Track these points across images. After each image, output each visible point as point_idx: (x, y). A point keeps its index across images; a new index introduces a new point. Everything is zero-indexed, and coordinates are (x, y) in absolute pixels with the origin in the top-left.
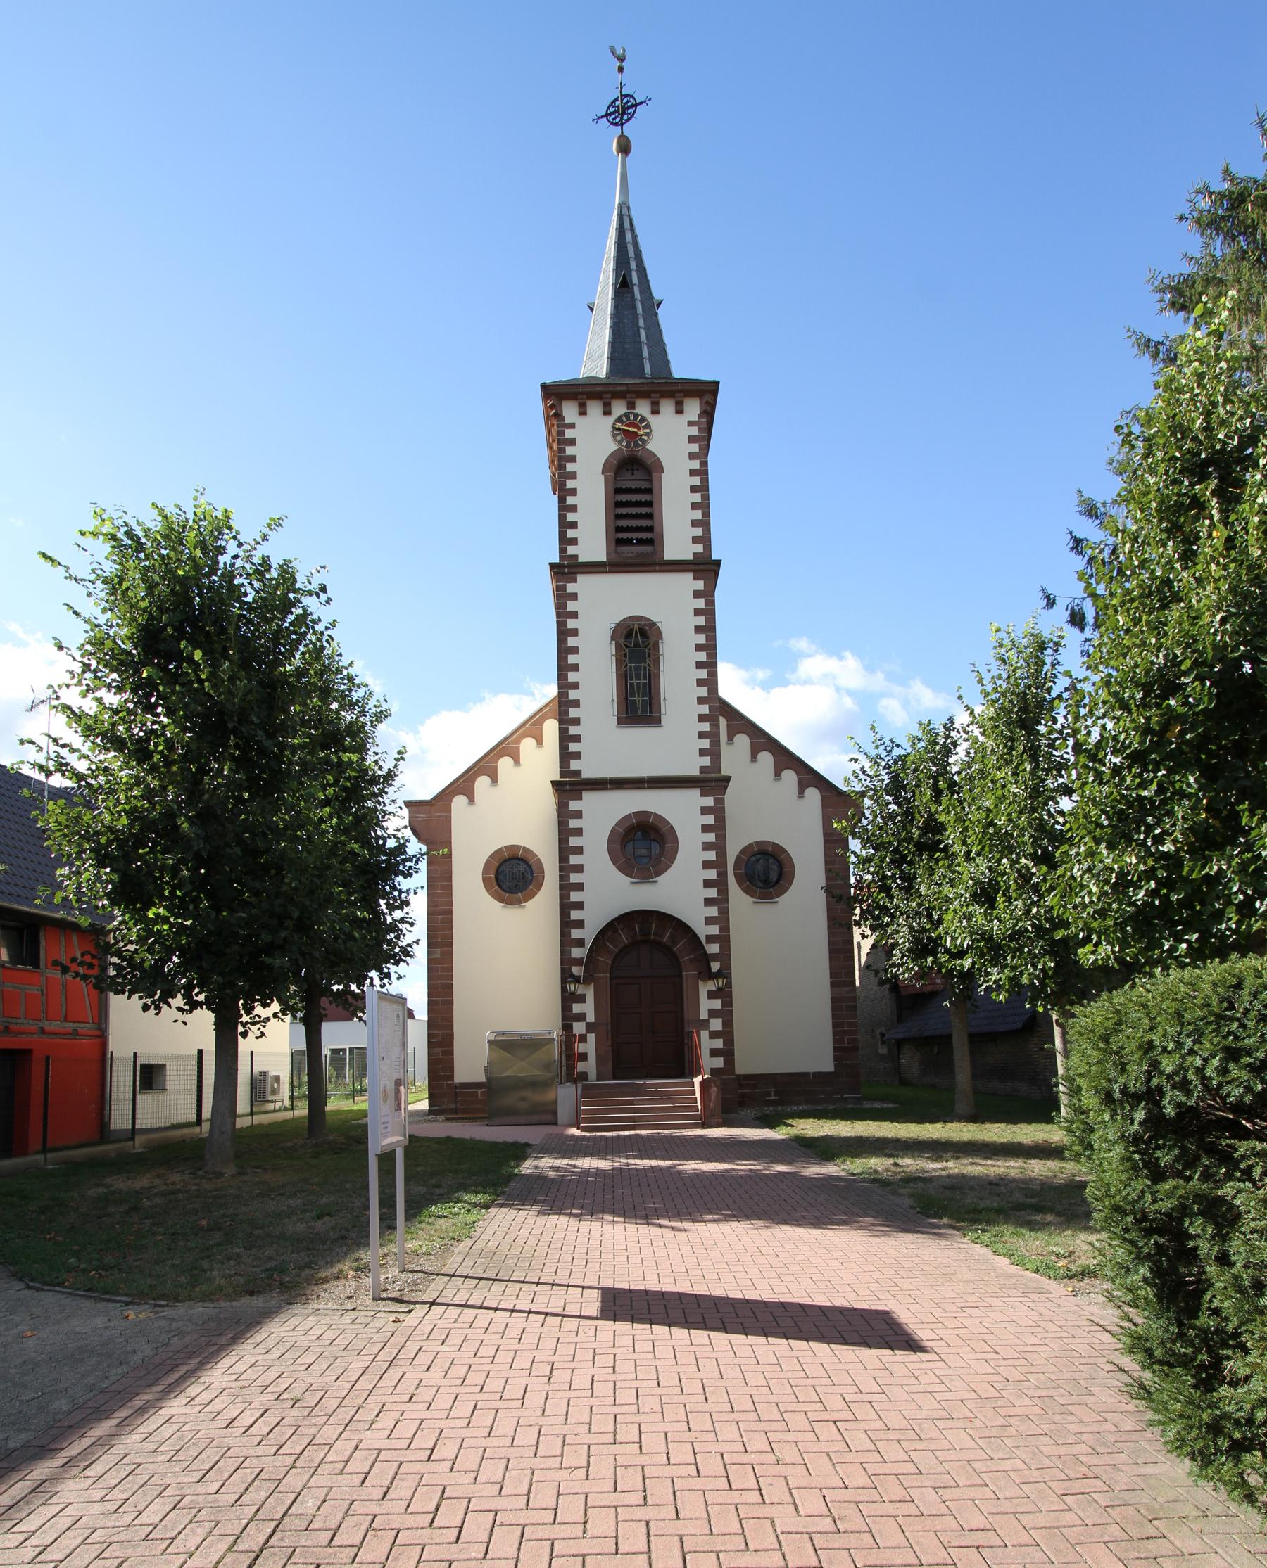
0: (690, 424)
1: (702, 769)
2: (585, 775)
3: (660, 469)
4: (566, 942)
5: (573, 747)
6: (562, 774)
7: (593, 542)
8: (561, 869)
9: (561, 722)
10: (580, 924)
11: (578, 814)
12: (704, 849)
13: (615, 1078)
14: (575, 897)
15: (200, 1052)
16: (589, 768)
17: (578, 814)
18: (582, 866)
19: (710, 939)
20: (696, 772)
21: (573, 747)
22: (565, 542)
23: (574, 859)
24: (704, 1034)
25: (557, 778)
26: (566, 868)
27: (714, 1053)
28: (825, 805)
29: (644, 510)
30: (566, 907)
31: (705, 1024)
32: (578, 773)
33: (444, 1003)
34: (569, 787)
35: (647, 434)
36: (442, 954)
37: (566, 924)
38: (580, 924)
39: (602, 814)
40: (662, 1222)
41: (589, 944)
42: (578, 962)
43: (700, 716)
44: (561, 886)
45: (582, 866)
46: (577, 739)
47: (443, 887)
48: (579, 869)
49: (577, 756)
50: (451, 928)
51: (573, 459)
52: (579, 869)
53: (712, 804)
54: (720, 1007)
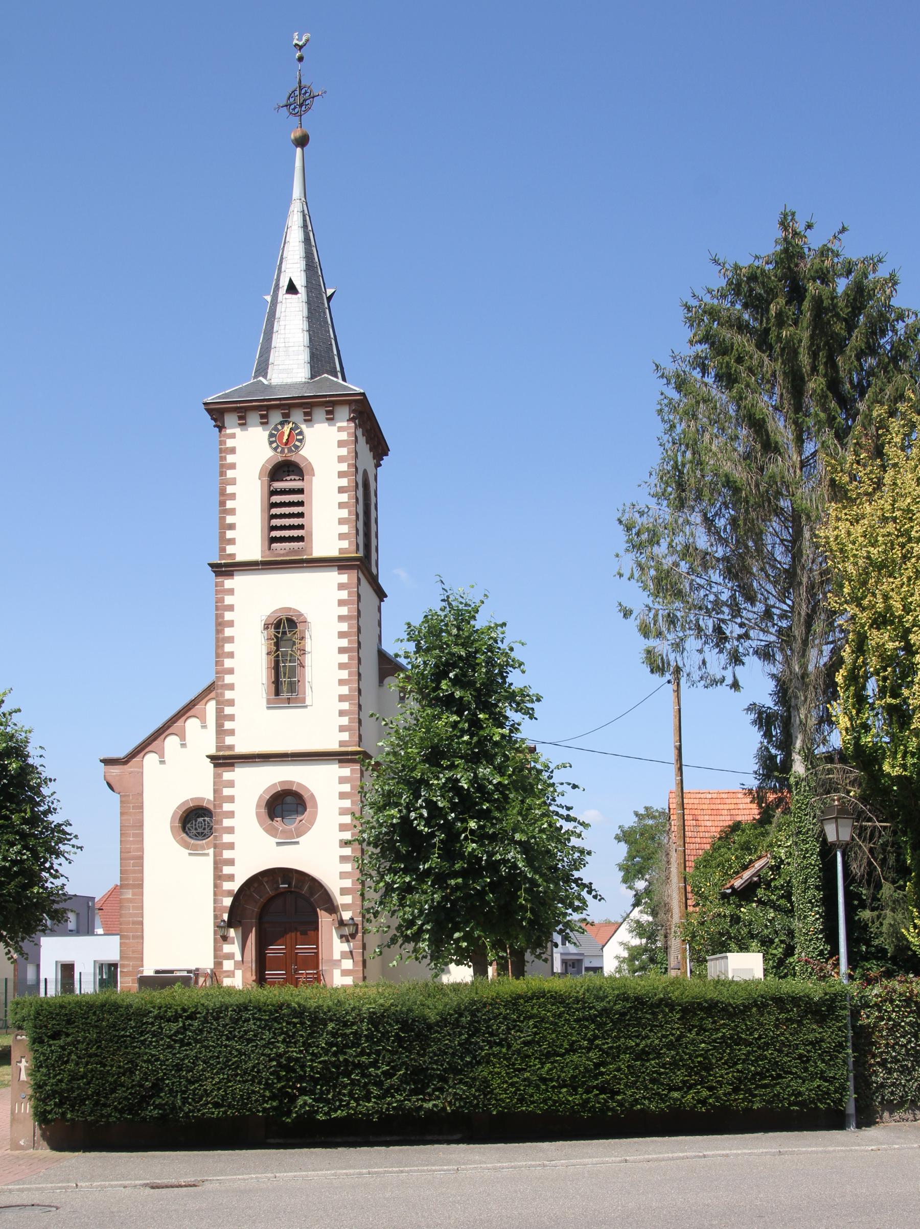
0: (340, 429)
6: (218, 748)
7: (248, 542)
9: (218, 703)
10: (231, 878)
11: (231, 784)
12: (340, 731)
15: (6, 979)
17: (231, 784)
19: (344, 891)
22: (221, 732)
24: (337, 973)
25: (213, 751)
29: (296, 510)
32: (231, 747)
33: (134, 937)
34: (224, 760)
35: (300, 441)
36: (133, 894)
39: (251, 785)
40: (288, 478)
47: (135, 835)
49: (232, 732)
50: (142, 872)
51: (231, 608)
54: (350, 902)
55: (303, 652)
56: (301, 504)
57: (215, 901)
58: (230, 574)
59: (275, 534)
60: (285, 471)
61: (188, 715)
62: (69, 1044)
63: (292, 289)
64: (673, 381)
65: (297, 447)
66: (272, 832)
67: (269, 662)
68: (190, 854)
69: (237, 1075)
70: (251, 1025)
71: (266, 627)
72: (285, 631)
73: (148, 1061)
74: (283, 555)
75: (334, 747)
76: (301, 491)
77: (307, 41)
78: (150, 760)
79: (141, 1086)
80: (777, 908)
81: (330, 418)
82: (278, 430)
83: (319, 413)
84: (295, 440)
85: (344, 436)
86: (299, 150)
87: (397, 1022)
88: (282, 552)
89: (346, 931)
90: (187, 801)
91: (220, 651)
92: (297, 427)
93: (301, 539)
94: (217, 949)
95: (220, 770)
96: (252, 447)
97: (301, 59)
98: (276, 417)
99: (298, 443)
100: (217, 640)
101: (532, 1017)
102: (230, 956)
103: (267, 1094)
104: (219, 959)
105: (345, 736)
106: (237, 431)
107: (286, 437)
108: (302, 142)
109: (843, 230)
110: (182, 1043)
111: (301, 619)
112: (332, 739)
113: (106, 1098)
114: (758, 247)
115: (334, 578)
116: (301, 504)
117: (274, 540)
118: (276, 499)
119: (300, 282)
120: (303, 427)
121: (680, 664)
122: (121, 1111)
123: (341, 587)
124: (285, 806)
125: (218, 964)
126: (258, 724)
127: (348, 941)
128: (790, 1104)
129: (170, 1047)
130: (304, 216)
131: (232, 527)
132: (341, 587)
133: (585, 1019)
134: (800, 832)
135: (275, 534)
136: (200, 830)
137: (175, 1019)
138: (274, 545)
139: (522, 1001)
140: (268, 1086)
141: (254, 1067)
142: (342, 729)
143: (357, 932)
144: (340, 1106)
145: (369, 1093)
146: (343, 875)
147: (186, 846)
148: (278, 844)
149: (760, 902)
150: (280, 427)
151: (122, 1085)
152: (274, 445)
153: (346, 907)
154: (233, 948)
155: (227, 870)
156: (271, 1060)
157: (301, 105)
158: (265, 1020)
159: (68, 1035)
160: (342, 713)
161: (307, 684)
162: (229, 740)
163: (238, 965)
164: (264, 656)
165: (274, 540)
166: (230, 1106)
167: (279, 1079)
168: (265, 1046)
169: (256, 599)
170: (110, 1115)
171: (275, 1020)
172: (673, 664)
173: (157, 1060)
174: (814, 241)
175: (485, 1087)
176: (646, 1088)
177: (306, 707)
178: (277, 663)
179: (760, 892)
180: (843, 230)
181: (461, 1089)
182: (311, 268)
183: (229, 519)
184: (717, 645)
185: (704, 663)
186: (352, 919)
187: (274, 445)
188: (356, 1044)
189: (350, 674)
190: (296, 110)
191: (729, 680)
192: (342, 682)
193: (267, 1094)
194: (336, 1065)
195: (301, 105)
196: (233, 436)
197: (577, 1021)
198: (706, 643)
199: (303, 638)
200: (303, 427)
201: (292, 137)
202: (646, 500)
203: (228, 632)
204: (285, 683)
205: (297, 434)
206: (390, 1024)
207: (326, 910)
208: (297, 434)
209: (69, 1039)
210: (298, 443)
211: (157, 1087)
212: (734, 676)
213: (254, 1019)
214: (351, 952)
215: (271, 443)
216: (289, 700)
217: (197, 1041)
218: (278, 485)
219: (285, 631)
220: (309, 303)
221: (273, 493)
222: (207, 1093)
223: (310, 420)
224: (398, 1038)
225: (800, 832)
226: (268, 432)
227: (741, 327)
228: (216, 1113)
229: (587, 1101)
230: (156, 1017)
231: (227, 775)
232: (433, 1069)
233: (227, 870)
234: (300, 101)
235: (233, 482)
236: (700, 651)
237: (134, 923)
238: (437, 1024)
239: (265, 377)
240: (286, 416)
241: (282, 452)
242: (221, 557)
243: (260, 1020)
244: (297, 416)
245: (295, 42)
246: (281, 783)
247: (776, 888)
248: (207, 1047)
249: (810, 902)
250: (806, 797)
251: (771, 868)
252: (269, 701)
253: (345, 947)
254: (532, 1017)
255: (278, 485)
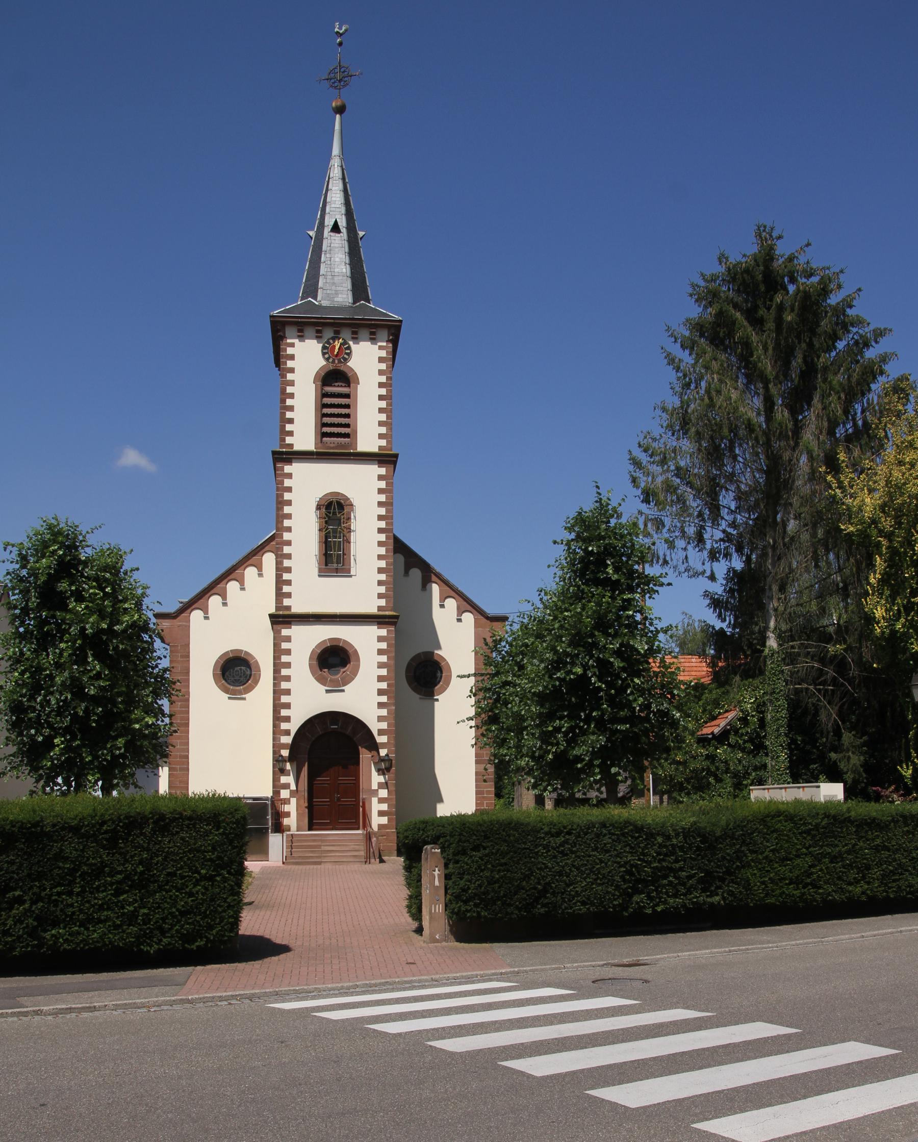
0: (381, 348)
1: (380, 448)
2: (296, 448)
3: (357, 382)
4: (277, 732)
5: (286, 589)
6: (277, 608)
7: (304, 435)
8: (275, 678)
10: (287, 719)
13: (310, 829)
14: (284, 699)
16: (297, 606)
18: (290, 581)
19: (381, 732)
20: (376, 450)
21: (286, 589)
22: (280, 595)
23: (284, 672)
24: (375, 800)
26: (278, 666)
27: (381, 813)
28: (477, 625)
30: (278, 706)
31: (375, 793)
32: (289, 608)
33: (181, 769)
34: (282, 619)
37: (278, 719)
38: (287, 719)
39: (306, 640)
41: (293, 734)
42: (284, 746)
43: (379, 569)
44: (274, 745)
45: (290, 581)
46: (289, 583)
48: (288, 679)
49: (289, 595)
50: (188, 712)
51: (289, 503)
52: (288, 679)
53: (386, 687)
54: (386, 741)
55: (349, 530)
56: (348, 416)
57: (274, 739)
58: (289, 461)
59: (325, 430)
60: (336, 380)
61: (229, 578)
62: (486, 855)
63: (336, 228)
64: (679, 341)
65: (345, 360)
66: (321, 680)
67: (320, 537)
68: (229, 698)
69: (598, 878)
70: (607, 840)
71: (319, 507)
72: (334, 512)
73: (540, 869)
74: (333, 448)
75: (373, 610)
76: (347, 396)
77: (346, 30)
78: (196, 616)
79: (535, 888)
80: (743, 750)
81: (373, 340)
82: (330, 344)
83: (364, 333)
84: (345, 353)
85: (383, 354)
86: (338, 116)
87: (699, 835)
88: (332, 445)
89: (383, 765)
90: (227, 653)
91: (280, 526)
92: (345, 343)
93: (347, 436)
94: (276, 780)
95: (278, 627)
96: (307, 357)
97: (340, 44)
98: (328, 333)
99: (346, 356)
100: (278, 516)
101: (775, 831)
102: (286, 786)
103: (617, 893)
104: (277, 787)
105: (383, 602)
106: (296, 341)
107: (336, 350)
108: (341, 110)
109: (808, 245)
110: (562, 852)
111: (347, 503)
112: (371, 604)
113: (511, 899)
114: (743, 249)
115: (376, 470)
116: (347, 406)
117: (325, 435)
118: (327, 400)
119: (342, 223)
120: (351, 343)
121: (668, 558)
122: (520, 909)
123: (380, 639)
124: (334, 661)
125: (276, 793)
126: (311, 591)
127: (384, 774)
128: (907, 894)
129: (555, 857)
130: (343, 170)
131: (291, 421)
132: (380, 639)
133: (805, 832)
134: (774, 692)
135: (325, 430)
136: (237, 678)
137: (558, 834)
138: (325, 439)
139: (768, 819)
140: (618, 887)
141: (609, 872)
142: (380, 596)
143: (391, 767)
144: (660, 901)
145: (678, 891)
146: (380, 719)
147: (226, 691)
148: (327, 691)
149: (729, 745)
150: (331, 341)
151: (523, 888)
152: (327, 356)
153: (384, 745)
154: (289, 779)
155: (284, 713)
156: (621, 866)
157: (340, 81)
158: (617, 835)
159: (485, 848)
160: (380, 583)
161: (352, 558)
162: (286, 602)
163: (293, 794)
164: (317, 532)
165: (325, 435)
166: (592, 904)
167: (624, 880)
168: (617, 856)
169: (309, 484)
170: (512, 913)
171: (623, 834)
172: (661, 557)
173: (547, 867)
174: (782, 250)
175: (747, 886)
176: (835, 884)
177: (351, 576)
178: (327, 537)
179: (732, 739)
180: (808, 245)
181: (733, 887)
182: (349, 214)
183: (289, 415)
184: (697, 545)
185: (686, 557)
186: (387, 755)
187: (327, 356)
188: (673, 853)
189: (387, 551)
190: (336, 84)
191: (708, 573)
192: (380, 557)
193: (617, 893)
194: (662, 868)
195: (340, 81)
196: (292, 345)
197: (800, 833)
198: (689, 543)
199: (349, 519)
200: (351, 343)
201: (334, 105)
202: (657, 431)
203: (287, 510)
204: (334, 557)
205: (346, 349)
206: (694, 838)
207: (367, 748)
208: (346, 349)
209: (487, 851)
210: (346, 356)
211: (545, 891)
212: (712, 571)
213: (610, 834)
214: (386, 783)
215: (324, 354)
216: (337, 570)
217: (572, 852)
218: (329, 389)
219: (334, 512)
220: (349, 241)
221: (325, 395)
222: (577, 894)
223: (356, 338)
224: (699, 848)
225: (774, 692)
226: (321, 345)
227: (736, 306)
228: (584, 909)
229: (803, 894)
230: (546, 833)
231: (285, 632)
232: (717, 872)
233: (284, 713)
234: (340, 78)
235: (292, 383)
236: (685, 549)
237: (181, 757)
238: (720, 837)
239: (315, 298)
240: (337, 332)
241: (333, 362)
242: (282, 446)
243: (613, 834)
244: (346, 333)
245: (336, 30)
246: (330, 640)
247: (742, 735)
248: (579, 857)
249: (781, 745)
250: (778, 666)
251: (739, 720)
252: (320, 570)
253: (381, 779)
254: (775, 831)
255: (329, 389)
